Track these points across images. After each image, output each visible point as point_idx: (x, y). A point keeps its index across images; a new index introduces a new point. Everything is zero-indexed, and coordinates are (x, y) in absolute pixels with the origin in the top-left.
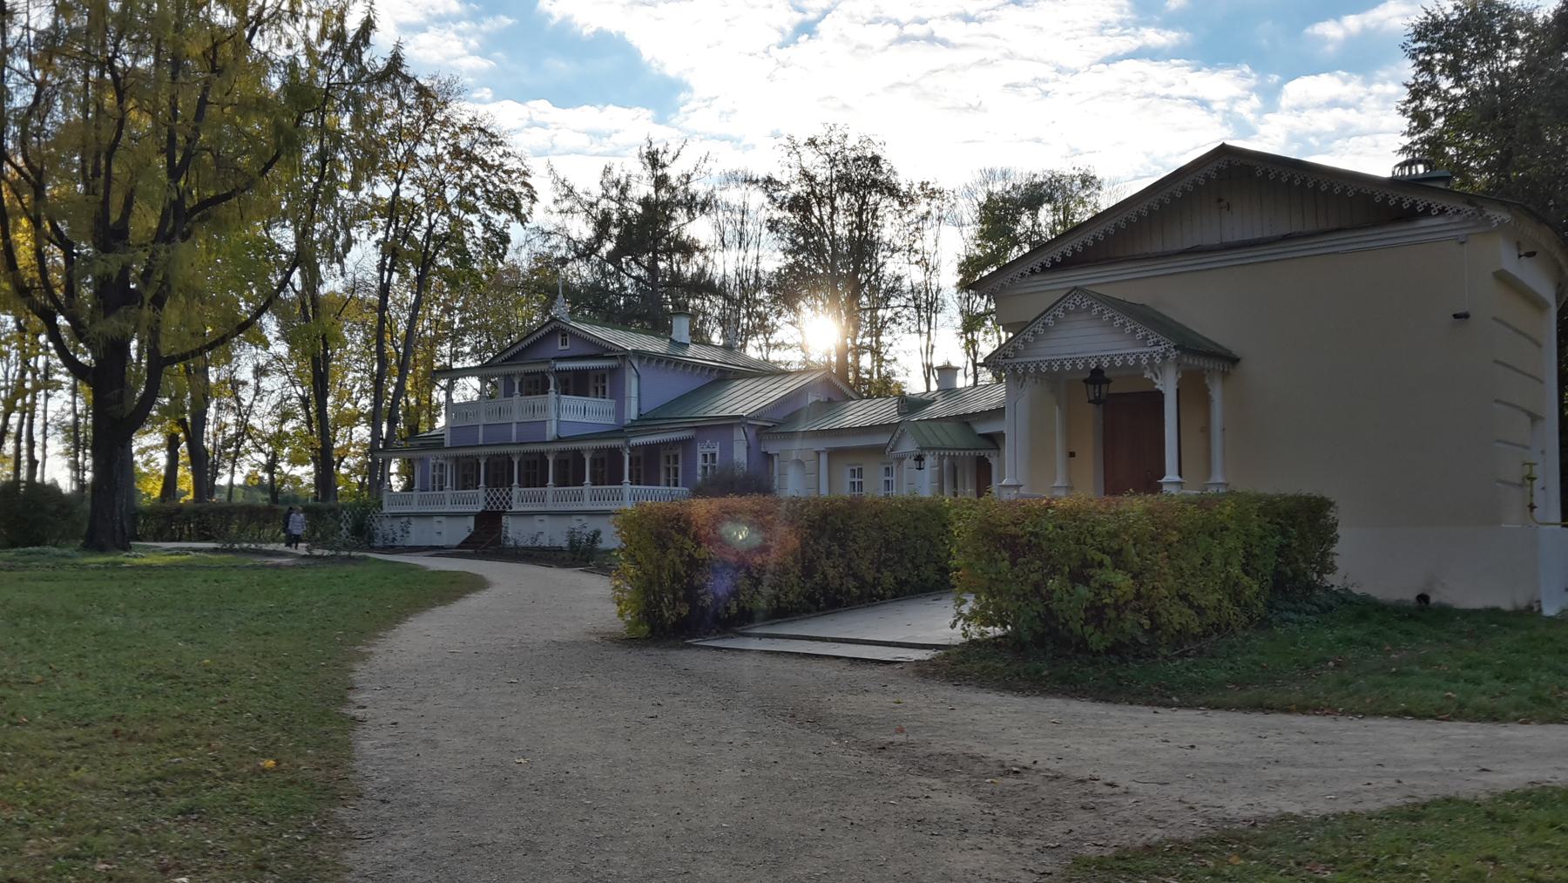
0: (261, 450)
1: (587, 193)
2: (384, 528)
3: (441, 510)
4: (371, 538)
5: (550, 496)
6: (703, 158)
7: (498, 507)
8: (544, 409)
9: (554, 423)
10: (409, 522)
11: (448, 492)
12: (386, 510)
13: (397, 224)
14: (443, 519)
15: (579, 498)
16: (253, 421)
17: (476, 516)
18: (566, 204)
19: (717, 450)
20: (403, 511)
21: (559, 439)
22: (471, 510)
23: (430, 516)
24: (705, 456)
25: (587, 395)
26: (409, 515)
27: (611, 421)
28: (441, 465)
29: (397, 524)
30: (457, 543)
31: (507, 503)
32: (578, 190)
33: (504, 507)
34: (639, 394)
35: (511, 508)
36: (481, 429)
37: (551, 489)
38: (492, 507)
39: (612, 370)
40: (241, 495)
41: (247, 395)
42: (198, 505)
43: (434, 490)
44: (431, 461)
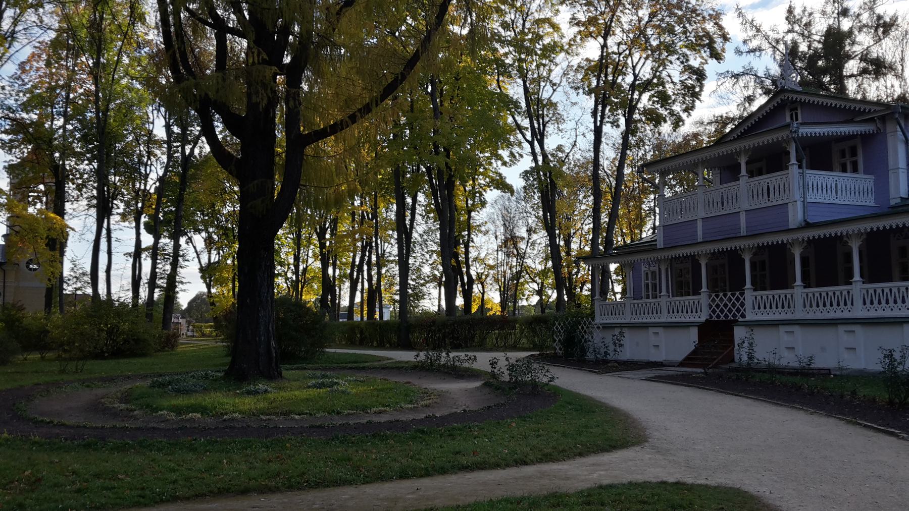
0: (534, 281)
1: (773, 30)
2: (598, 340)
3: (657, 320)
4: (584, 351)
5: (799, 301)
7: (726, 316)
8: (784, 189)
9: (799, 205)
10: (621, 333)
11: (664, 301)
12: (599, 320)
13: (606, 76)
14: (660, 330)
15: (848, 301)
16: (529, 262)
17: (698, 326)
20: (616, 321)
21: (807, 225)
22: (692, 319)
23: (645, 326)
25: (831, 170)
26: (621, 326)
27: (869, 201)
28: (653, 273)
29: (608, 337)
30: (680, 357)
31: (738, 310)
32: (765, 28)
33: (735, 316)
35: (743, 316)
36: (700, 224)
37: (798, 291)
38: (718, 316)
39: (866, 138)
40: (533, 311)
41: (522, 245)
42: (371, 321)
44: (643, 269)
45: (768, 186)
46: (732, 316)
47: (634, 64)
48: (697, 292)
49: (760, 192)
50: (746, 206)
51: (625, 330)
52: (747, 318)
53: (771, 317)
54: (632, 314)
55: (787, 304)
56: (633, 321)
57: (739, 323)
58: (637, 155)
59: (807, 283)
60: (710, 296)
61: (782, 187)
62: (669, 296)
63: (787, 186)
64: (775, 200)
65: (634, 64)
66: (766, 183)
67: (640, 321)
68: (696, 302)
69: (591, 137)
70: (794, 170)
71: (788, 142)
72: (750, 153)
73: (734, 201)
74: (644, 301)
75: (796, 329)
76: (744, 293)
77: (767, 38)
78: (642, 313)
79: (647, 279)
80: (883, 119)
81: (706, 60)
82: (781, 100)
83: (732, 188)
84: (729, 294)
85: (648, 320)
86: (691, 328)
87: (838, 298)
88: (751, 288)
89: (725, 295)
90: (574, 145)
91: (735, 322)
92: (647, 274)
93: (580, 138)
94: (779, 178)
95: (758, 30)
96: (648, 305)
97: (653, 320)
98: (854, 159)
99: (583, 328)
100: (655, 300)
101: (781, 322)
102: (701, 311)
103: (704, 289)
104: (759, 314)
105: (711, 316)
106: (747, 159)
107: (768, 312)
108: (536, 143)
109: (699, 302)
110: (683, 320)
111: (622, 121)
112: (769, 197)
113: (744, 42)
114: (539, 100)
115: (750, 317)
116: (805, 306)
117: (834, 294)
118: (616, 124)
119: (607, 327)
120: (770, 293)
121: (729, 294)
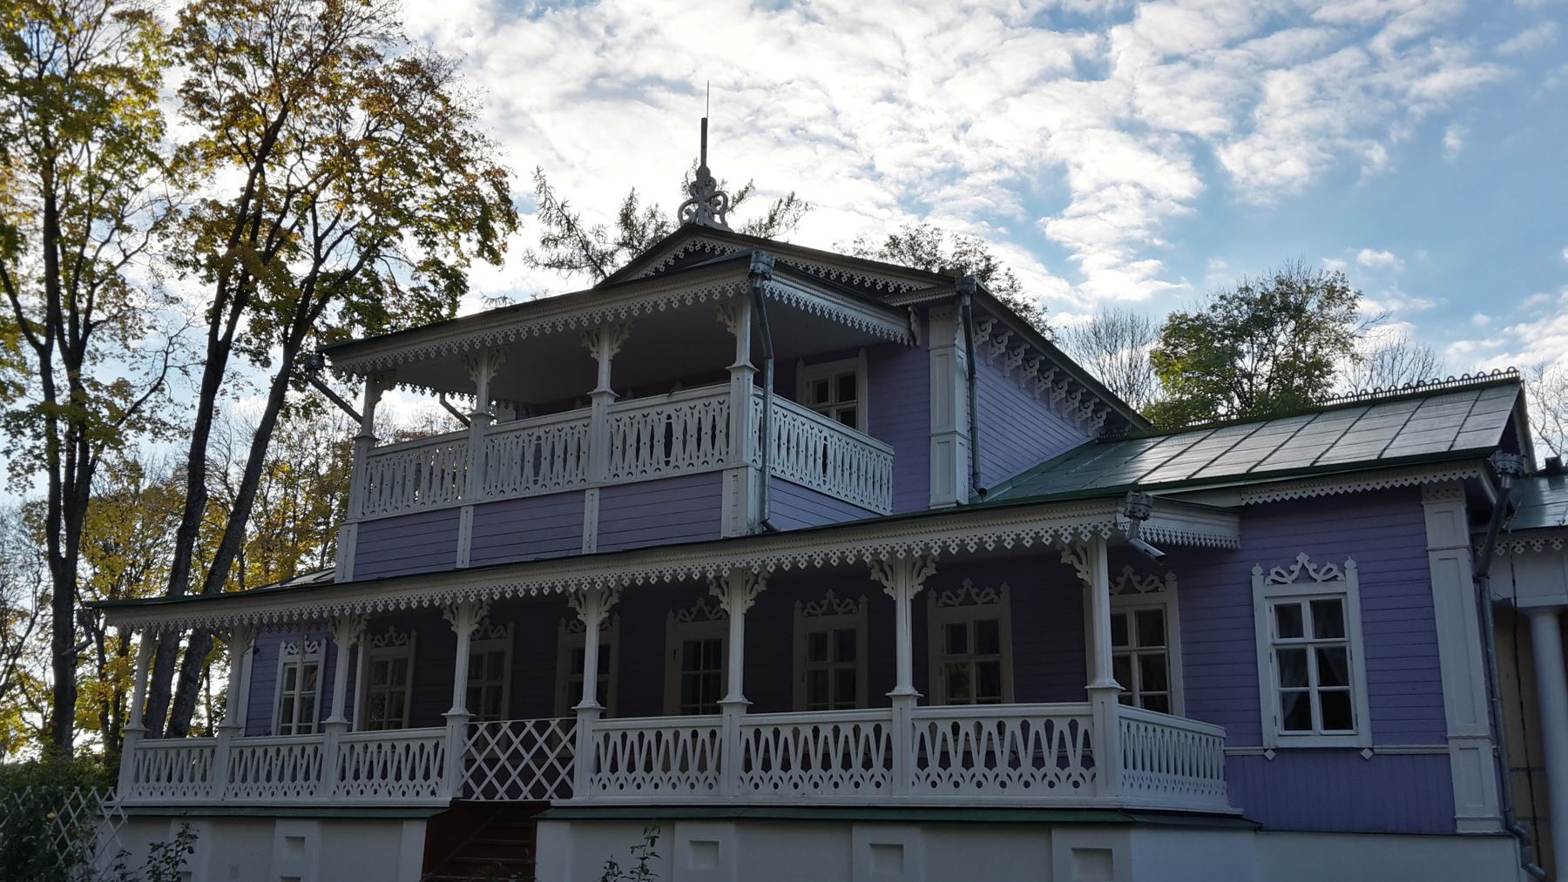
3: (305, 799)
6: (785, 200)
8: (717, 432)
10: (187, 840)
12: (128, 793)
14: (310, 831)
15: (310, 770)
17: (430, 821)
18: (564, 251)
19: (1348, 587)
21: (767, 534)
22: (411, 799)
23: (265, 817)
24: (1288, 618)
26: (186, 814)
31: (551, 774)
33: (538, 790)
34: (973, 429)
35: (565, 791)
36: (466, 522)
38: (490, 791)
39: (882, 353)
43: (288, 731)
45: (669, 426)
46: (507, 792)
47: (319, 235)
48: (881, 699)
49: (645, 438)
50: (601, 473)
51: (196, 828)
52: (579, 798)
53: (647, 796)
54: (232, 780)
55: (705, 757)
56: (231, 800)
57: (549, 813)
58: (301, 463)
59: (762, 697)
60: (472, 730)
61: (707, 428)
62: (350, 730)
63: (721, 426)
64: (684, 462)
65: (319, 235)
66: (664, 416)
67: (254, 799)
68: (429, 747)
69: (198, 374)
70: (743, 383)
71: (731, 306)
72: (626, 336)
73: (571, 460)
74: (275, 739)
75: (726, 835)
76: (575, 721)
77: (585, 245)
78: (263, 775)
79: (291, 686)
80: (924, 313)
81: (468, 260)
82: (686, 251)
83: (566, 426)
84: (506, 726)
85: (279, 799)
86: (407, 826)
87: (826, 743)
88: (743, 704)
89: (494, 730)
90: (157, 387)
91: (538, 811)
92: (292, 672)
93: (173, 374)
94: (699, 404)
95: (571, 226)
96: (284, 751)
97: (292, 799)
98: (847, 405)
99: (66, 818)
100: (305, 738)
101: (681, 813)
102: (440, 775)
103: (458, 707)
104: (613, 788)
105: (467, 790)
106: (617, 350)
107: (639, 780)
108: (56, 356)
109: (437, 745)
110: (382, 799)
111: (277, 353)
112: (668, 454)
113: (543, 242)
114: (82, 266)
115: (584, 793)
116: (748, 766)
117: (816, 731)
118: (262, 358)
119: (143, 817)
120: (1011, 711)
121: (506, 726)
